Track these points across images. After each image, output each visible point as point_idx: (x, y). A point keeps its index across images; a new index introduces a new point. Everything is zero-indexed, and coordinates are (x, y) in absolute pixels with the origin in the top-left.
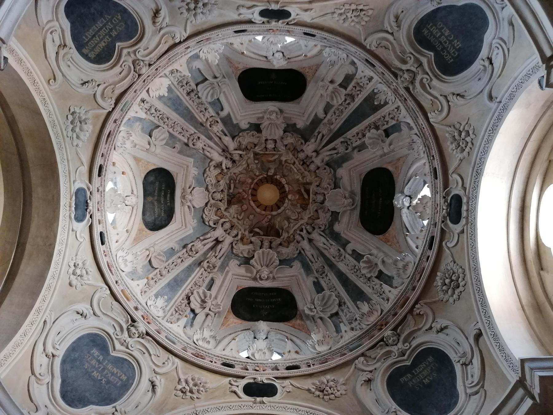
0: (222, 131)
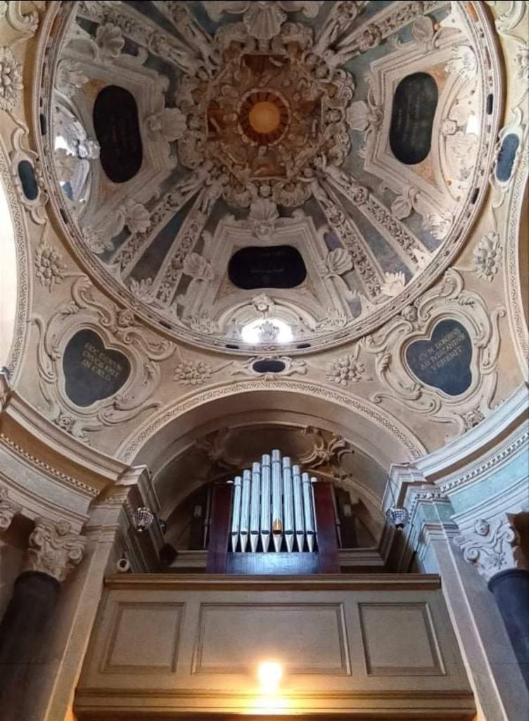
0: (326, 207)
